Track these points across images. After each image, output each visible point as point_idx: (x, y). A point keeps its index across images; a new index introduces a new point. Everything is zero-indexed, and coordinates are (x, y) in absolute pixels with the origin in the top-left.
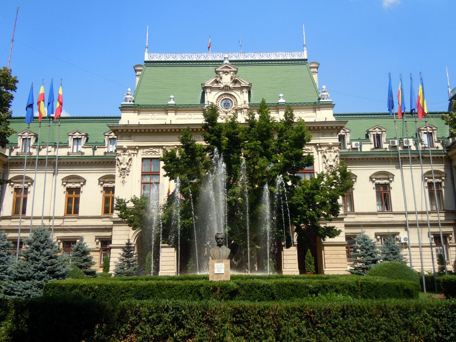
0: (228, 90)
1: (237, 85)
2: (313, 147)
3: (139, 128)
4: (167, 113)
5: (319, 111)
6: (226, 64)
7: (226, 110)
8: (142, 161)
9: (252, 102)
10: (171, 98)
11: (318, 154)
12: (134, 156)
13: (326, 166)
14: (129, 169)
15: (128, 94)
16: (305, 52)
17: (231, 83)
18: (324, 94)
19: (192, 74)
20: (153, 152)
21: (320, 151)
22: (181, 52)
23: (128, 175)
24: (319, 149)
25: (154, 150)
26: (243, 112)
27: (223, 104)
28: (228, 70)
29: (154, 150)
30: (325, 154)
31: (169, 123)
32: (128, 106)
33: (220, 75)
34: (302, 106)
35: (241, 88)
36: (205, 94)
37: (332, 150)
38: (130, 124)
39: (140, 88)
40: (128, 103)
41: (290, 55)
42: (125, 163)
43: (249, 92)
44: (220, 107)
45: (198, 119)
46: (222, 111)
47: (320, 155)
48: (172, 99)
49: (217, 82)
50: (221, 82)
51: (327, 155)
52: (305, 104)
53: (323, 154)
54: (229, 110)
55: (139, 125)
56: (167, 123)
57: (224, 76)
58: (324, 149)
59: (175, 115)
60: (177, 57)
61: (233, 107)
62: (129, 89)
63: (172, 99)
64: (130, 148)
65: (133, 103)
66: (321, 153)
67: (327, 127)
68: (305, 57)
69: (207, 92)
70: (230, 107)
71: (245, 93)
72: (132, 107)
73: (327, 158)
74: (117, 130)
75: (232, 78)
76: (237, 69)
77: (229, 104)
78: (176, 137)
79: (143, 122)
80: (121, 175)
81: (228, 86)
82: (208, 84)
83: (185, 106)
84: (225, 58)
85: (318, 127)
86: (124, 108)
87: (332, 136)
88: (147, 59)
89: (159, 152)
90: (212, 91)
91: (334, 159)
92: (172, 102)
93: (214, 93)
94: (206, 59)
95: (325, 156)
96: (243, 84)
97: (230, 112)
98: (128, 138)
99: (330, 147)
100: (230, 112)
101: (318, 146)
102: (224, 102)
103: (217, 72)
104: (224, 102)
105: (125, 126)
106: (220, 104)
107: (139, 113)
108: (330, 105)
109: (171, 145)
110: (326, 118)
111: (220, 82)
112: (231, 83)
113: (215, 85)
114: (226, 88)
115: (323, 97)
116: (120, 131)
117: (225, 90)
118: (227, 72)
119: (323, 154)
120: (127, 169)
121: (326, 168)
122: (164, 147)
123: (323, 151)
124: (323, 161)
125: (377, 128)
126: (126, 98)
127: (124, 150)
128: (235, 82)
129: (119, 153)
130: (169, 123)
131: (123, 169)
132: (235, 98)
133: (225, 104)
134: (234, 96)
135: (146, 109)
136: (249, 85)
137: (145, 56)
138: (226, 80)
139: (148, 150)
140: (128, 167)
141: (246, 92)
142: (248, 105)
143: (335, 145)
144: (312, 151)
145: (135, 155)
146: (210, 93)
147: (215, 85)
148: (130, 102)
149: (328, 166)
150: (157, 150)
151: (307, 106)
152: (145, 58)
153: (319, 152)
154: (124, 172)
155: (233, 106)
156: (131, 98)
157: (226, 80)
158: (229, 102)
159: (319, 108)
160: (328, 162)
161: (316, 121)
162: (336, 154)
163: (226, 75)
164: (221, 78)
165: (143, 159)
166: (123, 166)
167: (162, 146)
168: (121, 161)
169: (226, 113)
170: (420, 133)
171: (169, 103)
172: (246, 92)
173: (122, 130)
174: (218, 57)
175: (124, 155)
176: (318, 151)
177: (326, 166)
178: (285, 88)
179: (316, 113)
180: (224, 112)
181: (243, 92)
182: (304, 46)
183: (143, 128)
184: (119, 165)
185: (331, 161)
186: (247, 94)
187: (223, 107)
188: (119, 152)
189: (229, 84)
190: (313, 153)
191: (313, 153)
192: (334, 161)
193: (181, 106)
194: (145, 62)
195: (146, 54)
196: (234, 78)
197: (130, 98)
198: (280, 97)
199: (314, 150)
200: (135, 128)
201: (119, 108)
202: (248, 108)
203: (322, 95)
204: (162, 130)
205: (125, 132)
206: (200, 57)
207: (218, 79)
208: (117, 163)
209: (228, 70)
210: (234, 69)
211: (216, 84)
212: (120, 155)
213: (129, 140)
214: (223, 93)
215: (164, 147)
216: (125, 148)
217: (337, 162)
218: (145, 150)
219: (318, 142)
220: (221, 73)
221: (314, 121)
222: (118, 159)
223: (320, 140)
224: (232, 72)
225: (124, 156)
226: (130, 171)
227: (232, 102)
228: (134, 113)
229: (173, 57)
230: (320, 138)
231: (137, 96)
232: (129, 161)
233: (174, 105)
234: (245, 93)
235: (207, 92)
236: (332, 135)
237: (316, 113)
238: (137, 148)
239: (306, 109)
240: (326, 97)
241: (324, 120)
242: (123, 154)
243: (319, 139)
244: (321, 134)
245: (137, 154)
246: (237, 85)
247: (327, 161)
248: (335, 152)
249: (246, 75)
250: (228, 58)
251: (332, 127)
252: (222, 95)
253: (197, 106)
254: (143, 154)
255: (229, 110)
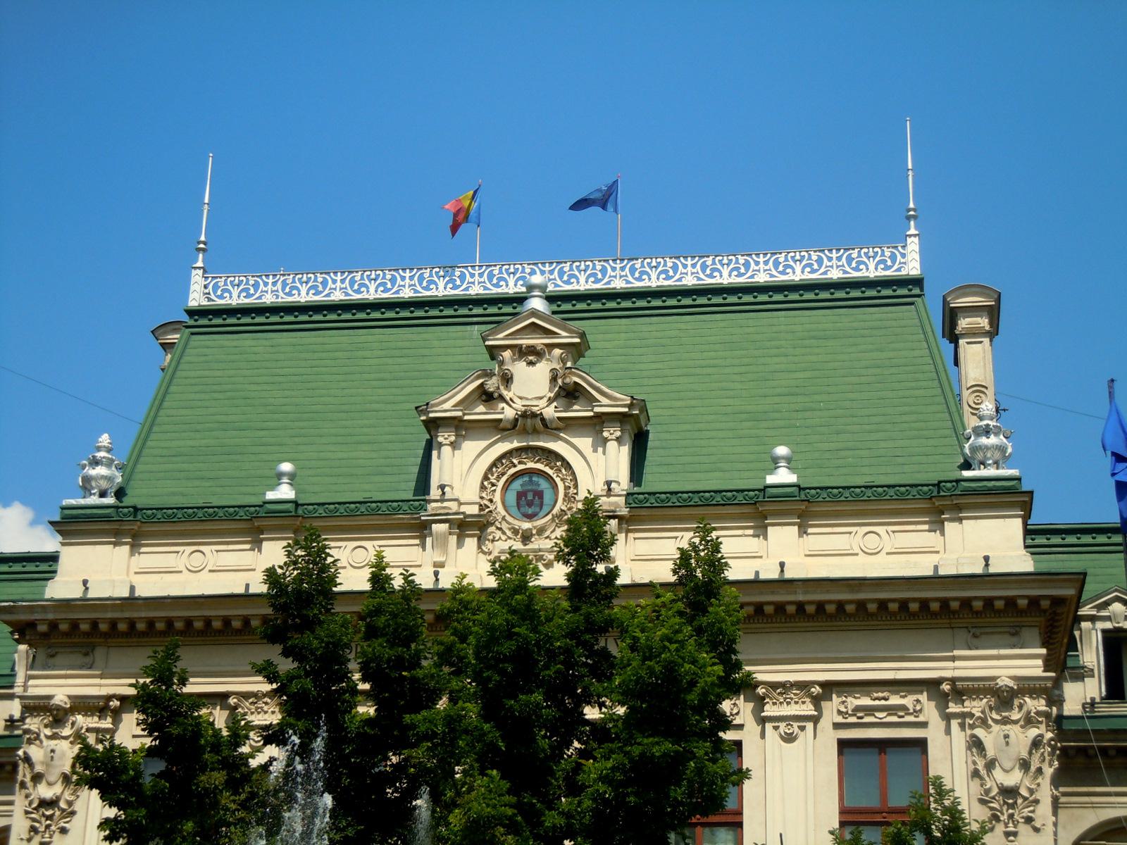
0: (535, 432)
1: (578, 411)
2: (923, 697)
3: (127, 615)
4: (761, 531)
5: (956, 524)
6: (534, 313)
7: (526, 525)
8: (840, 753)
9: (654, 481)
10: (280, 475)
11: (948, 731)
12: (802, 728)
13: (987, 792)
14: (70, 803)
15: (95, 462)
16: (913, 245)
17: (551, 401)
18: (984, 441)
19: (390, 361)
20: (892, 710)
21: (955, 716)
22: (772, 246)
23: (64, 831)
24: (953, 708)
25: (895, 700)
26: (429, 540)
27: (512, 497)
28: (538, 341)
29: (895, 700)
30: (980, 732)
31: (430, 586)
32: (100, 516)
33: (502, 363)
34: (212, 519)
35: (596, 424)
36: (435, 453)
37: (1015, 715)
38: (91, 595)
39: (155, 429)
40: (94, 500)
41: (279, 285)
42: (54, 775)
43: (639, 444)
44: (500, 509)
45: (236, 570)
46: (504, 526)
47: (959, 737)
48: (285, 480)
49: (487, 397)
50: (507, 395)
51: (990, 738)
52: (891, 492)
53: (969, 732)
54: (540, 523)
55: (132, 601)
56: (762, 576)
57: (519, 369)
58: (976, 706)
59: (800, 535)
60: (399, 281)
61: (556, 510)
62: (105, 439)
63: (285, 480)
64: (82, 705)
65: (110, 500)
66: (962, 726)
67: (989, 602)
68: (912, 267)
69: (440, 445)
70: (546, 509)
71: (612, 445)
72: (106, 519)
73: (991, 753)
74: (32, 625)
75: (554, 379)
76: (582, 335)
77: (539, 494)
78: (1014, 636)
79: (149, 588)
80: (34, 830)
81: (534, 415)
82: (446, 407)
83: (342, 509)
84: (531, 288)
85: (945, 602)
86: (74, 525)
87: (1013, 646)
88: (196, 299)
89: (917, 713)
90: (465, 438)
91: (1025, 754)
92: (783, 476)
93: (471, 447)
94: (888, 273)
95: (976, 745)
96: (604, 406)
97: (541, 531)
98: (79, 659)
99: (1004, 698)
100: (541, 531)
101: (946, 695)
102: (517, 485)
103: (493, 352)
104: (517, 485)
105: (66, 604)
106: (497, 497)
107: (135, 548)
108: (1007, 497)
109: (792, 678)
110: (986, 559)
111: (501, 398)
112: (551, 401)
113: (480, 412)
114: (529, 422)
115: (980, 456)
116: (42, 628)
117: (525, 432)
118: (532, 350)
119: (969, 732)
120: (63, 805)
121: (982, 802)
122: (232, 701)
123: (971, 715)
124: (972, 767)
125: (1117, 599)
126: (87, 480)
127: (58, 717)
128: (570, 394)
129: (34, 728)
130: (774, 575)
131: (44, 804)
132: (568, 466)
133: (520, 495)
134: (563, 459)
135: (188, 527)
136: (631, 406)
137: (192, 288)
138: (531, 385)
139: (866, 701)
140: (67, 796)
141: (618, 439)
142: (622, 500)
143: (1027, 687)
144: (921, 719)
145: (810, 726)
146: (455, 446)
147: (480, 412)
148: (103, 494)
149: (995, 791)
150: (908, 701)
151: (901, 499)
152: (191, 296)
153: (955, 724)
154: (49, 818)
155: (560, 505)
156: (109, 479)
157: (531, 385)
158: (544, 485)
159: (959, 508)
160: (998, 774)
161: (942, 572)
162: (1033, 732)
163: (531, 363)
164: (507, 380)
165: (843, 745)
166: (45, 791)
167: (224, 696)
168: (39, 768)
169: (526, 538)
170: (1077, 633)
171: (771, 479)
172: (618, 439)
173: (53, 625)
174: (304, 289)
175: (54, 737)
176: (948, 718)
177: (987, 792)
178: (808, 414)
179: (943, 534)
180: (516, 532)
181: (606, 440)
182: (909, 218)
183: (143, 615)
184: (30, 784)
185: (1007, 765)
186: (625, 451)
187: (514, 510)
188: (33, 723)
189: (543, 403)
190: (924, 725)
191: (924, 725)
192: (1025, 765)
193: (321, 510)
194: (192, 313)
195: (197, 278)
196: (564, 376)
197: (103, 477)
198: (775, 460)
199: (930, 711)
200: (109, 615)
201: (52, 523)
202: (624, 511)
203: (974, 449)
204: (227, 621)
205: (66, 634)
206: (787, 266)
207: (492, 384)
208: (20, 778)
209: (538, 341)
210: (565, 338)
211: (481, 408)
212: (38, 737)
213: (81, 668)
214: (516, 444)
215: (232, 701)
216: (58, 708)
217: (1039, 771)
218: (853, 702)
219: (948, 674)
220: (507, 354)
221: (930, 573)
222: (27, 759)
223: (958, 663)
224: (557, 352)
225: (53, 743)
226: (73, 813)
227: (555, 486)
228: (115, 544)
229: (246, 290)
230: (956, 653)
231: (140, 467)
232: (1030, 753)
233: (290, 507)
234: (612, 445)
235: (440, 445)
236: (1014, 640)
237: (943, 534)
238: (115, 703)
239: (166, 535)
240: (991, 457)
241: (978, 569)
242: (48, 732)
243: (953, 659)
244: (962, 635)
245: (815, 720)
246: (578, 411)
247: (990, 765)
248: (1029, 721)
249: (624, 364)
250: (542, 288)
251: (1011, 602)
252: (508, 455)
253: (393, 506)
254: (840, 719)
255: (540, 523)
